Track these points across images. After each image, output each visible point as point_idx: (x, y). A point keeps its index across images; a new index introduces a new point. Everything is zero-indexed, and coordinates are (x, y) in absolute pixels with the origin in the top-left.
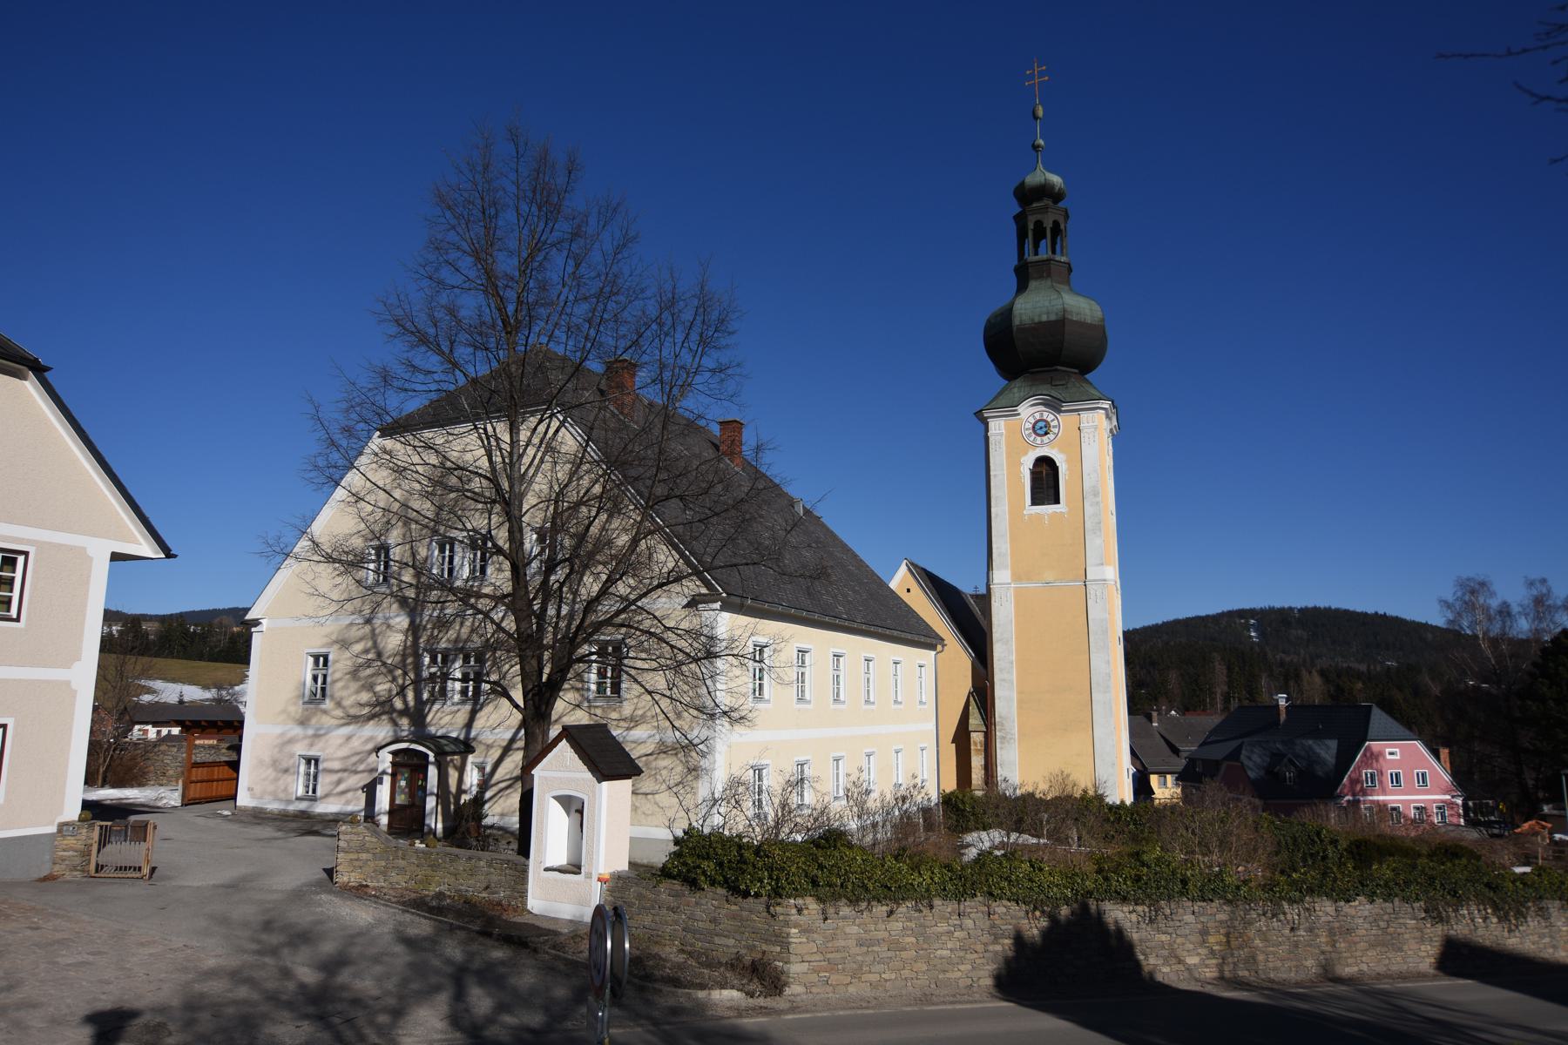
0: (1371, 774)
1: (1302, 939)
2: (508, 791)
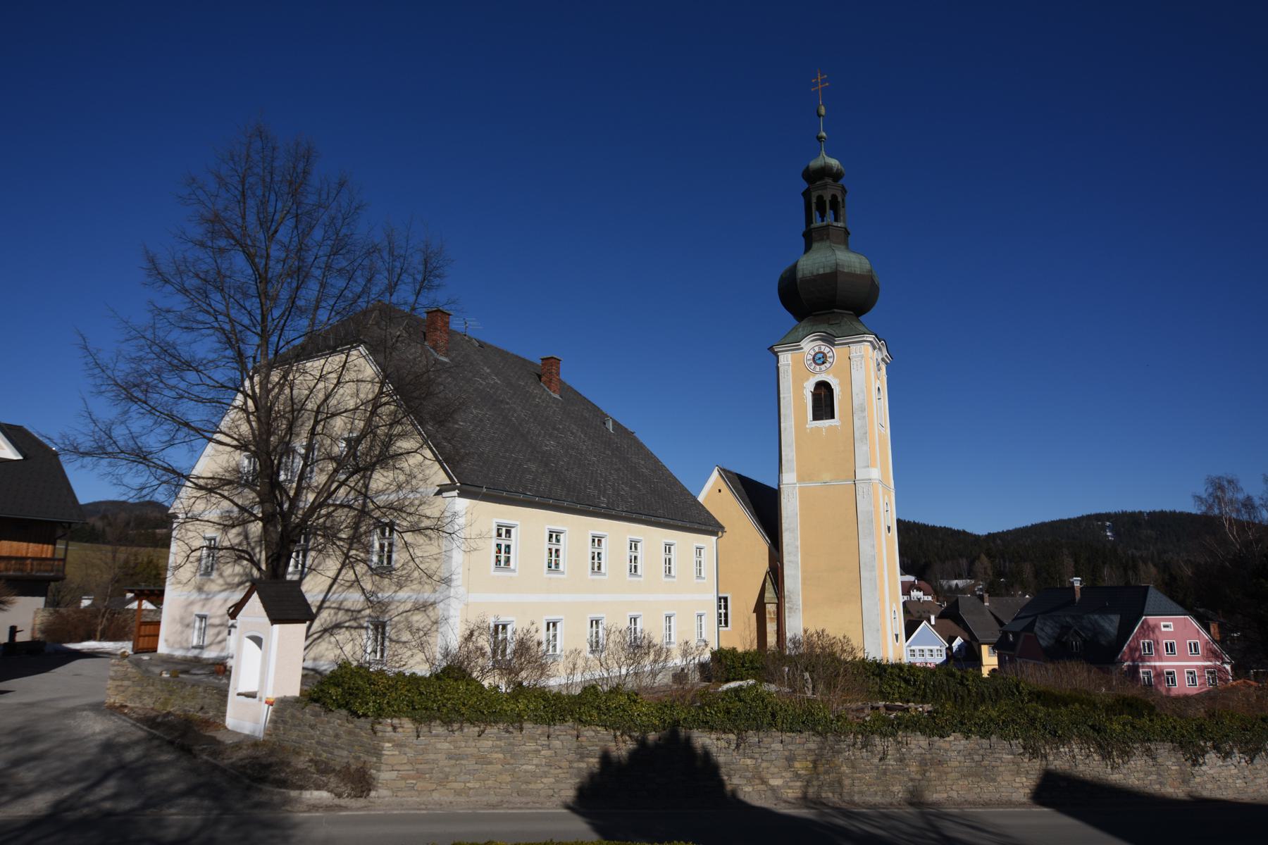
0: (1148, 644)
1: (891, 767)
2: (320, 640)
